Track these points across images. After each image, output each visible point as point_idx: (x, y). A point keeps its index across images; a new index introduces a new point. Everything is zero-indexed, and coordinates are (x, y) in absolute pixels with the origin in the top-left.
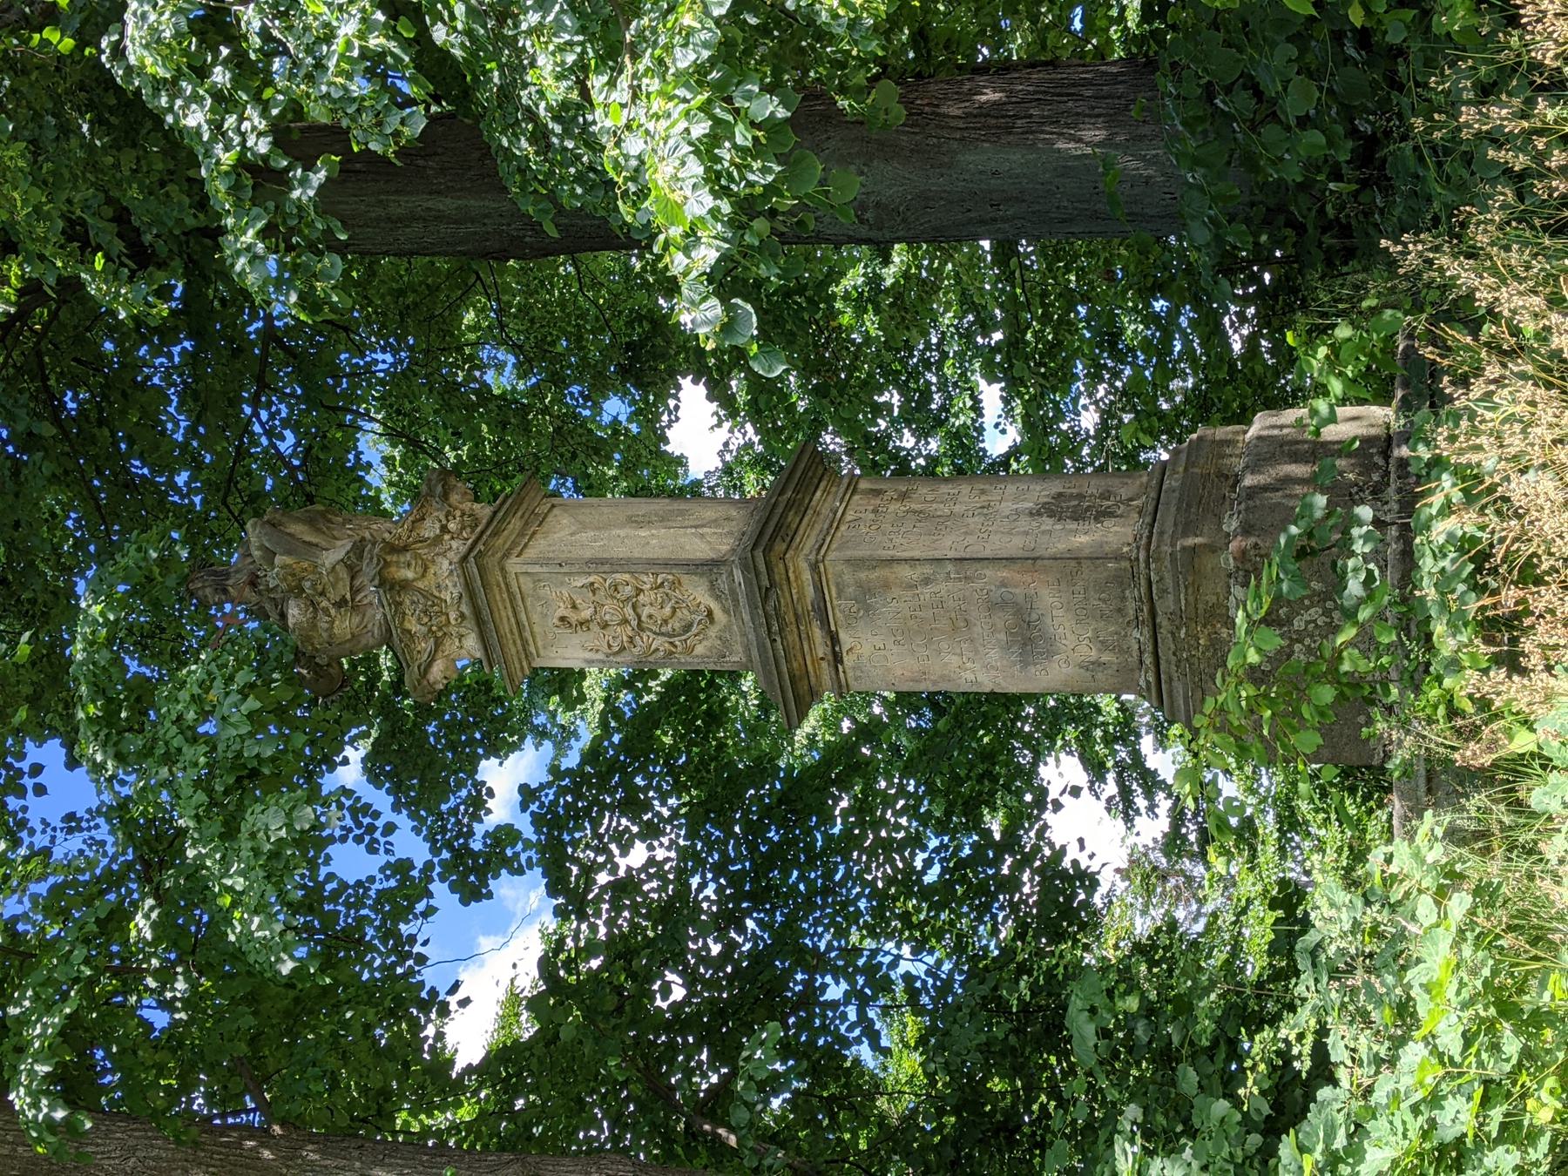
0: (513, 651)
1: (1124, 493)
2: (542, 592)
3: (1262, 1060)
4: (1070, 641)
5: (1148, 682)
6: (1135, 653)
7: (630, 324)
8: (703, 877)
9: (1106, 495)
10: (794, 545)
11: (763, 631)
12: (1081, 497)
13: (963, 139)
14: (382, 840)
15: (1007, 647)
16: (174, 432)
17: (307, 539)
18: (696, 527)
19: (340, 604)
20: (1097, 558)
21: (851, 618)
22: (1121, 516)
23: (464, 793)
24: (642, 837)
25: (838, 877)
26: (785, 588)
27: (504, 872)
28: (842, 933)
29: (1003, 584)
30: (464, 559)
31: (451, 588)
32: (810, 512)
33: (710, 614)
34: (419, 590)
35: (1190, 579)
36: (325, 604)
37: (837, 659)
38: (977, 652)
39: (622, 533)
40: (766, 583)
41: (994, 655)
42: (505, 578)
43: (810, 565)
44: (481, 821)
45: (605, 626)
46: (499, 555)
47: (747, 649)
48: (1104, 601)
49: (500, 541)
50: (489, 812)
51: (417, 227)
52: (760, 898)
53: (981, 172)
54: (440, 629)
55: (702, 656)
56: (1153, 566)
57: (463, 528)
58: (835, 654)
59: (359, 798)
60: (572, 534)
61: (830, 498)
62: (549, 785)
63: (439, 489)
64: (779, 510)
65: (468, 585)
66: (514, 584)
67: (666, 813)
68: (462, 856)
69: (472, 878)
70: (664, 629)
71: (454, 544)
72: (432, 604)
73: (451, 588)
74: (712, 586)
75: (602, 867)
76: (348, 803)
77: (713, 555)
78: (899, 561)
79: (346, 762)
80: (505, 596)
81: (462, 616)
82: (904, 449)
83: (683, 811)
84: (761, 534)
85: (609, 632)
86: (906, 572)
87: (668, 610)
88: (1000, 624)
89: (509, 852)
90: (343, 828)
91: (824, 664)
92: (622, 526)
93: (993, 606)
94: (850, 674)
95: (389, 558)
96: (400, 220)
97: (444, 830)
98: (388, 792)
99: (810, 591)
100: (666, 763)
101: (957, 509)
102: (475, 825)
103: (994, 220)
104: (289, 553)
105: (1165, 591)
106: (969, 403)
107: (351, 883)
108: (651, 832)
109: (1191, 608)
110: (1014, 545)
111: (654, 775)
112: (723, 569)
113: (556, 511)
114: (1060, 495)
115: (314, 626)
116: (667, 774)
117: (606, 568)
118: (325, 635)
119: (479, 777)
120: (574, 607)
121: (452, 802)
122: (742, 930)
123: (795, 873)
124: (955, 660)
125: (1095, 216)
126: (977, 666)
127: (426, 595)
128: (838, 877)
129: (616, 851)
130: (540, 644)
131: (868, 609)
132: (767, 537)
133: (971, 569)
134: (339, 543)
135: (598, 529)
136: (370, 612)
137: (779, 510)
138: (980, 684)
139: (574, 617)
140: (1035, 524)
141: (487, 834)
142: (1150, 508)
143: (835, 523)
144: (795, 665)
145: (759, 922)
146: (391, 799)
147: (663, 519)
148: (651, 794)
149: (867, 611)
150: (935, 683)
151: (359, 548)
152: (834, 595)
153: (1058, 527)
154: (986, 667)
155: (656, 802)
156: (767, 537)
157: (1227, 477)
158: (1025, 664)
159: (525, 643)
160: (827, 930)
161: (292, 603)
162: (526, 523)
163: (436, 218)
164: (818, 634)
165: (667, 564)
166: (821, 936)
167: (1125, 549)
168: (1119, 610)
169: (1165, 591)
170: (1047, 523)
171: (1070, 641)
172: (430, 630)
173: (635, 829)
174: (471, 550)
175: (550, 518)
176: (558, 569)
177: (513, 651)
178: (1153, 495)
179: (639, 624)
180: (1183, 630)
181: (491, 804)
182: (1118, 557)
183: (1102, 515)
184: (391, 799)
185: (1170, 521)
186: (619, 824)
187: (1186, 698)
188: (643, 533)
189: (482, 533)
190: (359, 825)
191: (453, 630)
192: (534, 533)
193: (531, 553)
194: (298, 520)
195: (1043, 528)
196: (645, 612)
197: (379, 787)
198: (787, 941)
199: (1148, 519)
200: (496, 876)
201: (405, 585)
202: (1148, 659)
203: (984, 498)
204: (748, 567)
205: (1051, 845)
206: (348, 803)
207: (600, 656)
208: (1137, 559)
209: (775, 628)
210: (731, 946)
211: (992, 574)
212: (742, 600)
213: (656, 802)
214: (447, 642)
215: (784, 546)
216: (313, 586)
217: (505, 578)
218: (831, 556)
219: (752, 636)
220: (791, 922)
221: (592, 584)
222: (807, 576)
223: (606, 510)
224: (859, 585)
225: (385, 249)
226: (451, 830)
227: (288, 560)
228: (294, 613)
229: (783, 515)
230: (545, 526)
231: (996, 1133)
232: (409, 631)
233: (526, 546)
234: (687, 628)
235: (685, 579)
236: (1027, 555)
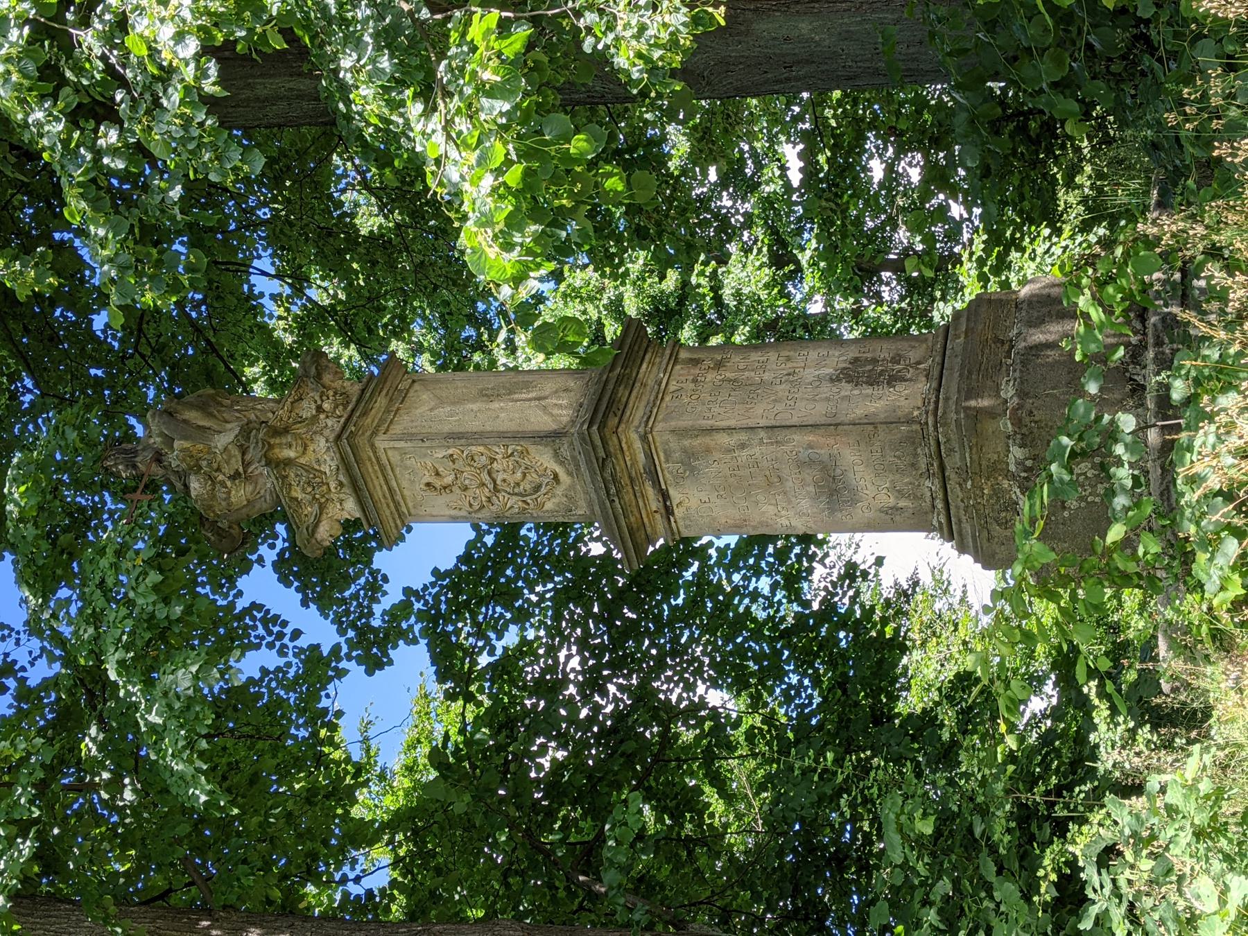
1: (914, 356)
2: (408, 462)
3: (1053, 869)
4: (871, 491)
5: (940, 523)
6: (928, 499)
8: (569, 649)
9: (896, 359)
10: (625, 418)
11: (603, 493)
12: (874, 361)
13: (756, 10)
14: (291, 645)
15: (815, 498)
16: (91, 277)
17: (201, 423)
19: (235, 476)
20: (891, 423)
21: (679, 479)
22: (910, 380)
23: (362, 581)
24: (513, 621)
25: (683, 641)
26: (620, 456)
27: (401, 642)
28: (690, 687)
29: (810, 446)
30: (339, 437)
31: (329, 462)
32: (638, 385)
33: (556, 477)
34: (302, 466)
35: (974, 441)
36: (221, 477)
37: (669, 512)
38: (790, 502)
39: (475, 407)
40: (602, 454)
41: (805, 504)
42: (375, 453)
43: (640, 437)
44: (379, 602)
45: (466, 489)
46: (369, 433)
47: (590, 504)
48: (899, 458)
49: (369, 420)
50: (385, 593)
51: (283, 105)
52: (616, 666)
53: (775, 39)
55: (552, 511)
56: (940, 430)
57: (336, 407)
58: (666, 507)
59: (268, 611)
60: (431, 410)
61: (655, 368)
62: (433, 585)
64: (611, 386)
65: (343, 459)
66: (383, 457)
67: (534, 598)
68: (365, 634)
69: (375, 650)
70: (516, 490)
71: (330, 423)
72: (314, 477)
73: (329, 462)
74: (556, 454)
75: (482, 649)
76: (259, 616)
77: (554, 426)
78: (718, 430)
79: (261, 560)
80: (377, 468)
81: (341, 484)
82: (724, 207)
83: (548, 596)
84: (600, 400)
86: (724, 439)
87: (519, 475)
88: (809, 479)
89: (404, 625)
90: (256, 637)
91: (658, 516)
92: (474, 400)
93: (801, 464)
94: (681, 523)
95: (272, 441)
96: (266, 99)
97: (347, 613)
98: (297, 590)
99: (641, 457)
100: (532, 557)
101: (767, 376)
102: (374, 606)
103: (788, 79)
104: (185, 438)
105: (952, 450)
106: (777, 173)
107: (272, 669)
108: (522, 617)
109: (976, 465)
110: (817, 412)
111: (521, 566)
112: (565, 440)
113: (417, 386)
114: (856, 360)
115: (213, 497)
116: (533, 565)
117: (463, 441)
119: (375, 566)
120: (437, 474)
121: (353, 589)
122: (604, 693)
123: (647, 642)
124: (771, 510)
125: (876, 72)
126: (791, 513)
127: (308, 469)
128: (683, 641)
129: (492, 635)
130: (410, 505)
131: (693, 470)
132: (600, 415)
133: (780, 435)
134: (229, 426)
135: (453, 403)
136: (261, 481)
137: (611, 386)
138: (795, 528)
139: (438, 483)
140: (835, 390)
141: (384, 612)
142: (936, 373)
143: (660, 394)
144: (632, 519)
145: (620, 688)
146: (300, 596)
148: (520, 584)
149: (692, 471)
150: (754, 528)
151: (246, 431)
152: (662, 458)
153: (856, 392)
154: (800, 514)
155: (526, 591)
156: (600, 415)
157: (1003, 343)
158: (832, 511)
159: (397, 505)
160: (677, 685)
161: (192, 478)
162: (391, 400)
163: (298, 97)
164: (650, 492)
165: (517, 436)
166: (672, 691)
167: (916, 413)
168: (913, 465)
169: (952, 450)
170: (846, 389)
171: (871, 491)
172: (314, 498)
173: (508, 616)
174: (344, 428)
175: (411, 394)
176: (420, 444)
178: (938, 359)
179: (495, 487)
180: (970, 483)
181: (386, 587)
182: (910, 421)
183: (893, 380)
184: (300, 596)
185: (954, 388)
186: (494, 612)
187: (974, 537)
188: (495, 405)
189: (353, 411)
190: (270, 633)
191: (334, 496)
192: (398, 409)
193: (397, 429)
194: (192, 406)
195: (843, 393)
197: (288, 585)
198: (643, 696)
199: (935, 384)
200: (395, 647)
201: (288, 462)
202: (940, 505)
203: (790, 365)
204: (586, 439)
205: (862, 606)
206: (259, 616)
207: (463, 513)
208: (927, 423)
210: (597, 708)
211: (798, 438)
213: (526, 591)
215: (617, 420)
216: (209, 465)
217: (375, 453)
218: (659, 427)
219: (594, 496)
220: (644, 684)
222: (638, 445)
223: (459, 384)
224: (684, 450)
225: (256, 123)
226: (355, 612)
227: (186, 444)
228: (196, 486)
229: (614, 392)
230: (407, 403)
231: (828, 863)
232: (296, 499)
233: (391, 422)
234: (537, 488)
235: (532, 449)
236: (829, 421)
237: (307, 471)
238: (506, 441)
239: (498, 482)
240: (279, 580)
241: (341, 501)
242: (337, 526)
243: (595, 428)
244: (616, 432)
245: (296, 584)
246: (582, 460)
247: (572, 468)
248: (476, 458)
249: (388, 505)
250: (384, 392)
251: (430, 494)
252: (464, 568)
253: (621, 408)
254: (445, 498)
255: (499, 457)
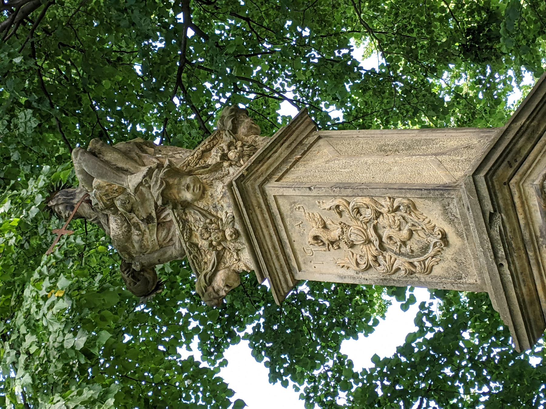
0: (277, 266)
2: (298, 213)
7: (470, 13)
11: (490, 254)
17: (120, 165)
18: (436, 155)
19: (148, 220)
33: (444, 237)
36: (135, 219)
39: (370, 160)
40: (489, 208)
42: (266, 200)
47: (481, 273)
54: (219, 244)
55: (441, 277)
63: (229, 124)
71: (231, 170)
73: (226, 209)
74: (445, 211)
80: (267, 216)
85: (357, 251)
87: (405, 233)
92: (372, 154)
95: (171, 181)
97: (315, 389)
98: (266, 364)
112: (454, 194)
113: (321, 142)
116: (471, 368)
117: (349, 192)
118: (136, 246)
119: (343, 351)
120: (325, 227)
121: (322, 370)
127: (205, 213)
130: (301, 260)
139: (324, 237)
147: (410, 148)
148: (457, 384)
155: (461, 390)
165: (402, 189)
172: (211, 245)
176: (308, 192)
177: (277, 266)
184: (268, 370)
191: (231, 245)
192: (297, 161)
193: (289, 178)
196: (385, 234)
209: (501, 253)
212: (472, 225)
214: (227, 255)
221: (338, 207)
223: (362, 141)
226: (322, 390)
230: (306, 157)
232: (196, 245)
233: (287, 172)
234: (425, 249)
237: (204, 215)
238: (392, 194)
239: (384, 239)
240: (253, 354)
241: (238, 251)
242: (233, 276)
243: (482, 175)
244: (507, 184)
245: (266, 359)
246: (470, 216)
247: (462, 227)
248: (362, 210)
249: (277, 257)
250: (286, 144)
251: (318, 249)
252: (403, 359)
253: (519, 160)
254: (333, 253)
255: (384, 210)
